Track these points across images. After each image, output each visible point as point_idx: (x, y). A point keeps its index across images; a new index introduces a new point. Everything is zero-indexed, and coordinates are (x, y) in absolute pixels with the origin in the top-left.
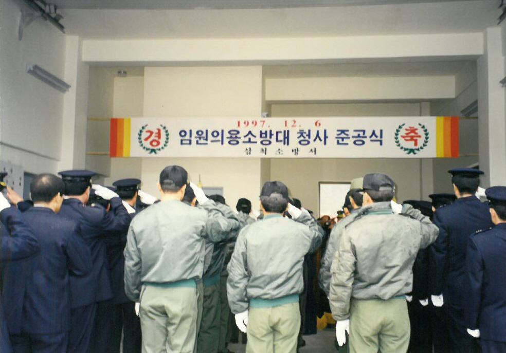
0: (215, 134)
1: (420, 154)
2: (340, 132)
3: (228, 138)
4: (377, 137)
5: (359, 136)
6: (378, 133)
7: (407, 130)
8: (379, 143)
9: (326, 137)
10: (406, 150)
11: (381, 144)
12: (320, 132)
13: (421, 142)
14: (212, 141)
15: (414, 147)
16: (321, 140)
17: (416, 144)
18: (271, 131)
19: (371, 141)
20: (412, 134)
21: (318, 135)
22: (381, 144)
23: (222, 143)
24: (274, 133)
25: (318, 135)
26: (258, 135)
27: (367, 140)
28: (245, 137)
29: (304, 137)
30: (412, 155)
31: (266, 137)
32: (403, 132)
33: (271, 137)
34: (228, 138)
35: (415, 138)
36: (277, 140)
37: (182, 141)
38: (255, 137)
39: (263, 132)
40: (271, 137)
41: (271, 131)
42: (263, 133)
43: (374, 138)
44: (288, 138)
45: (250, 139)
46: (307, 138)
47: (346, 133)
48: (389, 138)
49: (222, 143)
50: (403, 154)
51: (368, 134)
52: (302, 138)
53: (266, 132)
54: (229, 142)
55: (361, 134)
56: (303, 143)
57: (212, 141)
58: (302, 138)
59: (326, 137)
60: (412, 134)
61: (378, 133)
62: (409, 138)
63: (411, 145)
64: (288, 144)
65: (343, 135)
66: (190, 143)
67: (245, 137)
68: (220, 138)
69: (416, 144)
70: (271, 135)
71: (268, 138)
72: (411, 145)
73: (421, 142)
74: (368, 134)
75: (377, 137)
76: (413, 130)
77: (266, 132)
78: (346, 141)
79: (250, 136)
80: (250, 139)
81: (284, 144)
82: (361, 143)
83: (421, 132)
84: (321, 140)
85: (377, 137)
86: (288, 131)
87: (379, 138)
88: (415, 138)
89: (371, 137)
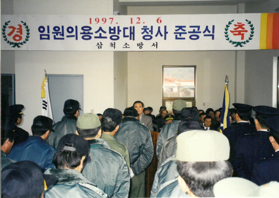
0: (70, 30)
1: (246, 47)
2: (178, 28)
3: (81, 33)
4: (209, 32)
5: (194, 31)
6: (210, 29)
7: (235, 25)
8: (211, 37)
9: (166, 33)
10: (234, 43)
11: (213, 39)
12: (191, 25)
13: (247, 36)
14: (68, 36)
15: (241, 41)
16: (162, 35)
17: (242, 38)
18: (118, 27)
19: (205, 35)
20: (240, 29)
21: (159, 31)
22: (213, 39)
23: (77, 39)
24: (121, 29)
25: (159, 31)
26: (107, 30)
27: (201, 35)
28: (96, 32)
29: (148, 33)
30: (239, 48)
31: (114, 33)
32: (232, 27)
33: (118, 34)
34: (81, 33)
35: (242, 33)
36: (125, 36)
37: (41, 35)
38: (105, 32)
39: (112, 28)
40: (118, 34)
41: (118, 27)
42: (112, 30)
43: (207, 33)
44: (134, 33)
45: (100, 34)
46: (150, 34)
47: (183, 28)
48: (219, 33)
49: (77, 39)
50: (232, 47)
51: (202, 29)
52: (145, 34)
53: (115, 28)
54: (83, 38)
55: (196, 29)
56: (113, 38)
57: (68, 36)
58: (145, 34)
59: (166, 33)
60: (240, 29)
61: (210, 29)
62: (237, 33)
63: (238, 39)
64: (134, 39)
65: (180, 31)
66: (48, 38)
67: (96, 32)
68: (74, 33)
69: (242, 38)
70: (119, 31)
71: (116, 34)
72: (238, 39)
73: (247, 36)
74: (202, 29)
75: (209, 32)
76: (241, 26)
77: (115, 28)
78: (183, 36)
79: (100, 32)
80: (100, 34)
81: (131, 39)
82: (88, 37)
83: (247, 27)
84: (162, 35)
85: (210, 32)
86: (134, 27)
87: (211, 33)
88: (242, 33)
89: (204, 32)
